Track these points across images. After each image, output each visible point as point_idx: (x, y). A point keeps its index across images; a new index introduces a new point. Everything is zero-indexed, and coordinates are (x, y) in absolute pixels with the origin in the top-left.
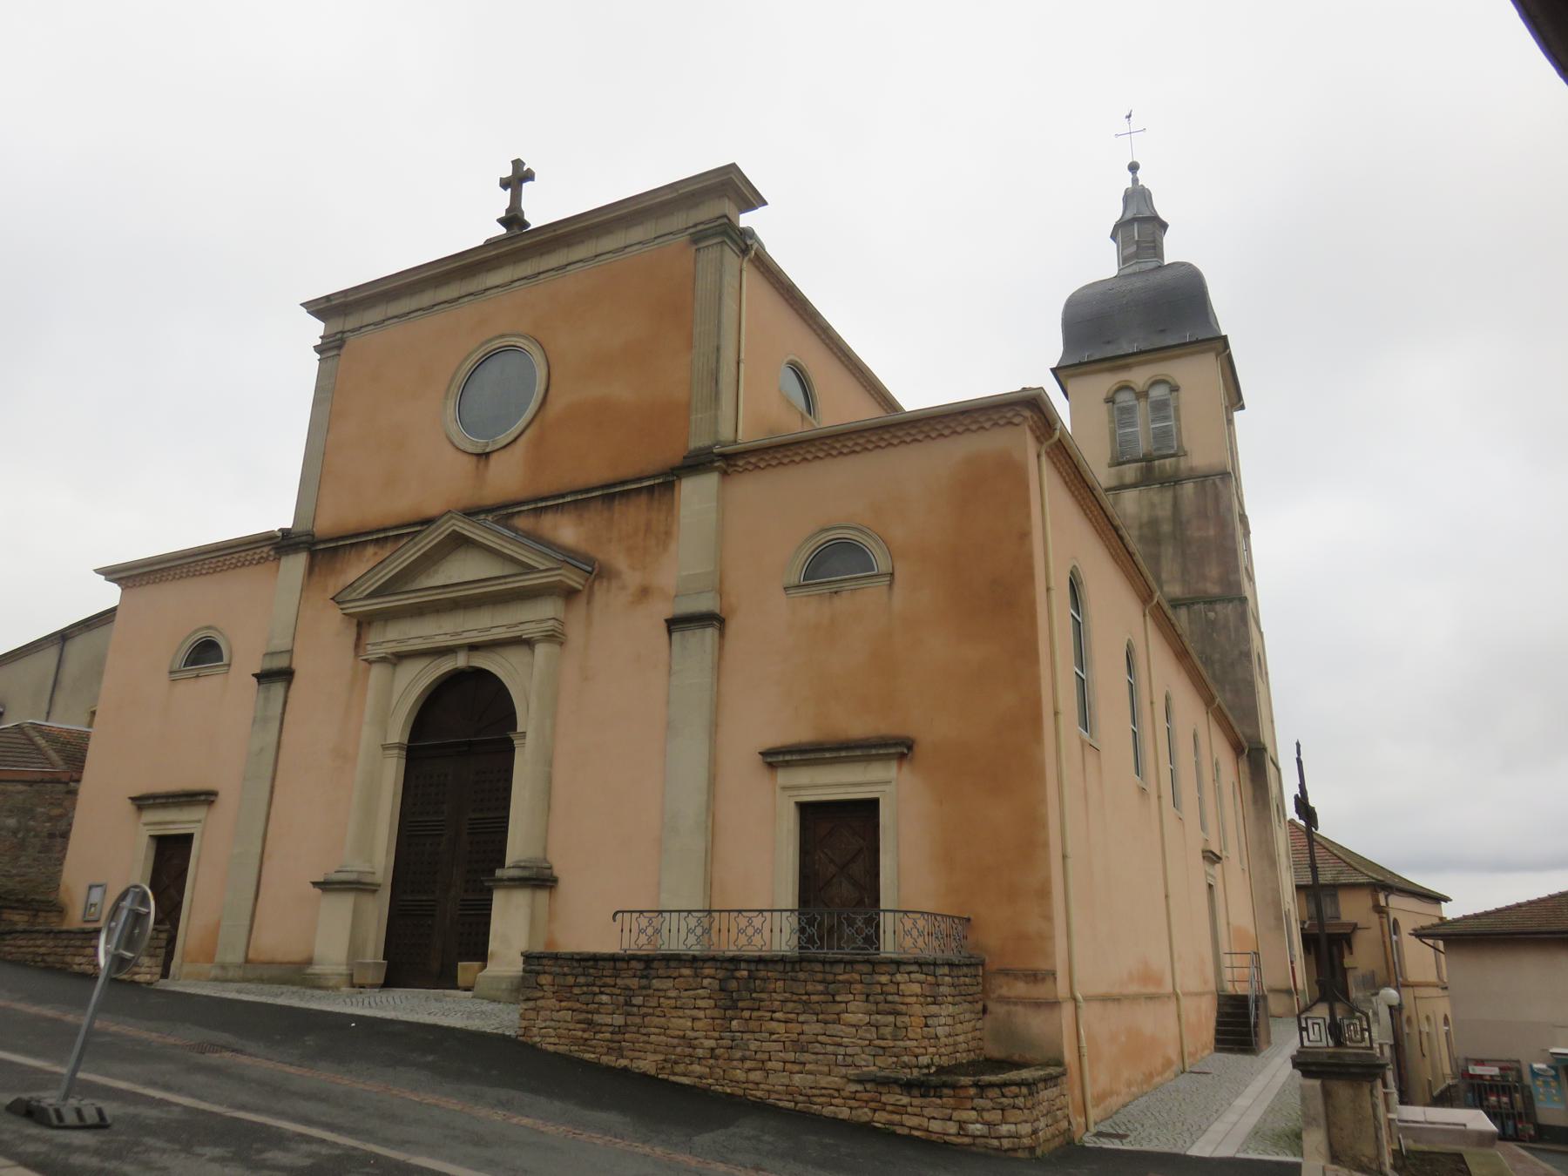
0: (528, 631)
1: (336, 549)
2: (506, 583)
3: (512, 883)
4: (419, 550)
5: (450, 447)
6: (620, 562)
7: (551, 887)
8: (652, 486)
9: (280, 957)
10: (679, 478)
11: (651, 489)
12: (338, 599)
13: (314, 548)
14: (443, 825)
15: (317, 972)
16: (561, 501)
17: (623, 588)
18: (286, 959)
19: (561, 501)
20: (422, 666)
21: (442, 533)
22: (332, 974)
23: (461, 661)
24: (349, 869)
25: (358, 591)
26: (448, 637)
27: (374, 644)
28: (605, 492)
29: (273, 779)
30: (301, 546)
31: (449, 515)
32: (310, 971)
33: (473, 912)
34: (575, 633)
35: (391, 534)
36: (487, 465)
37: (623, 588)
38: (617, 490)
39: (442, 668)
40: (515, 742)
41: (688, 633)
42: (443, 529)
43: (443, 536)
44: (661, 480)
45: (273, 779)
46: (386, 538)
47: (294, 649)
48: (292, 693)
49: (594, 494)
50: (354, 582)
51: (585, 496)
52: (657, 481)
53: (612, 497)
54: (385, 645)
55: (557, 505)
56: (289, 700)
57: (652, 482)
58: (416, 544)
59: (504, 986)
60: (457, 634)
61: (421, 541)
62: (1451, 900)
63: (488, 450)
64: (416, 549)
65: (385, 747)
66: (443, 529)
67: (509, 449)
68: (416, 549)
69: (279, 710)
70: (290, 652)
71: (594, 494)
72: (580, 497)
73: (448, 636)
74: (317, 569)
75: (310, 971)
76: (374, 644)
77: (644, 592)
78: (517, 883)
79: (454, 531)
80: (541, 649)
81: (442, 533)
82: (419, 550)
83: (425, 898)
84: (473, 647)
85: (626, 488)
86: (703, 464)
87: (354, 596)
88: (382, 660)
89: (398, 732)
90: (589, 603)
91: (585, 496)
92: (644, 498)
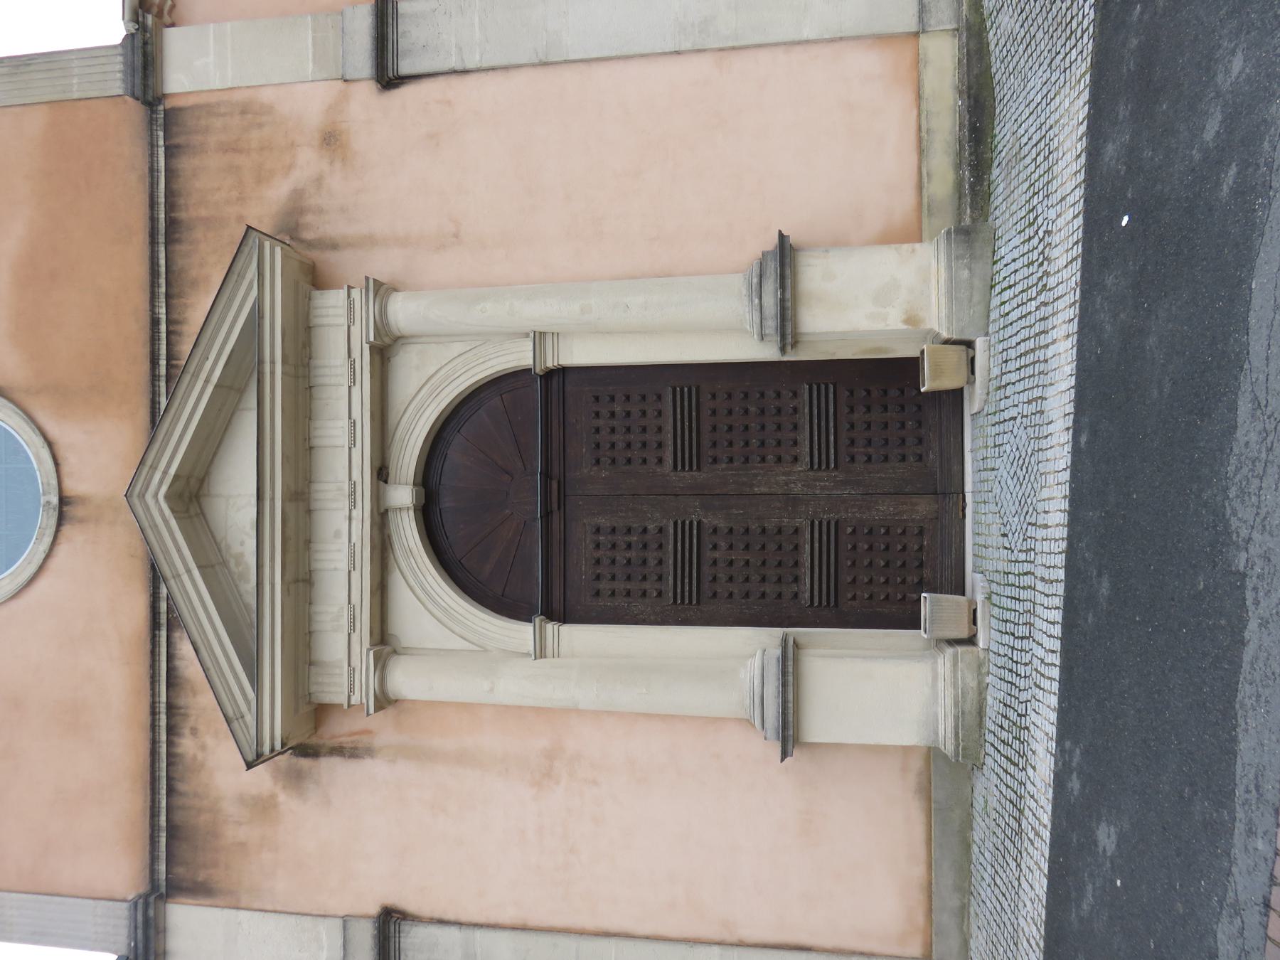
0: (362, 336)
1: (172, 830)
2: (273, 362)
3: (788, 282)
4: (189, 571)
5: (43, 584)
6: (278, 193)
7: (793, 249)
8: (167, 148)
9: (919, 871)
10: (161, 98)
11: (170, 152)
12: (251, 757)
13: (163, 890)
14: (683, 523)
15: (950, 735)
16: (163, 327)
17: (319, 181)
18: (921, 851)
19: (163, 327)
20: (397, 570)
21: (166, 521)
22: (955, 685)
23: (403, 495)
24: (757, 682)
25: (244, 707)
26: (356, 513)
27: (351, 689)
28: (162, 239)
29: (582, 933)
30: (151, 913)
31: (136, 501)
32: (949, 749)
33: (832, 451)
34: (382, 265)
35: (163, 698)
36: (82, 500)
37: (319, 181)
38: (162, 216)
39: (412, 545)
40: (550, 365)
41: (403, 44)
42: (159, 520)
43: (173, 523)
44: (161, 134)
45: (582, 933)
46: (170, 707)
47: (342, 913)
48: (425, 910)
49: (162, 262)
50: (225, 716)
51: (162, 281)
52: (161, 142)
53: (172, 223)
54: (356, 662)
55: (168, 333)
56: (437, 915)
57: (161, 151)
58: (177, 576)
59: (966, 273)
60: (353, 493)
61: (172, 565)
62: (780, 231)
63: (55, 500)
64: (185, 577)
65: (540, 652)
66: (159, 520)
67: (62, 453)
68: (185, 577)
69: (454, 932)
70: (346, 920)
71: (162, 262)
72: (163, 290)
73: (354, 513)
74: (201, 876)
75: (949, 749)
76: (351, 689)
77: (331, 140)
78: (788, 272)
79: (167, 497)
80: (403, 312)
81: (166, 521)
82: (189, 571)
83: (807, 547)
84: (382, 473)
85: (162, 200)
86: (145, 43)
87: (250, 719)
88: (381, 664)
89: (521, 633)
90: (334, 246)
91: (162, 281)
92: (185, 164)
